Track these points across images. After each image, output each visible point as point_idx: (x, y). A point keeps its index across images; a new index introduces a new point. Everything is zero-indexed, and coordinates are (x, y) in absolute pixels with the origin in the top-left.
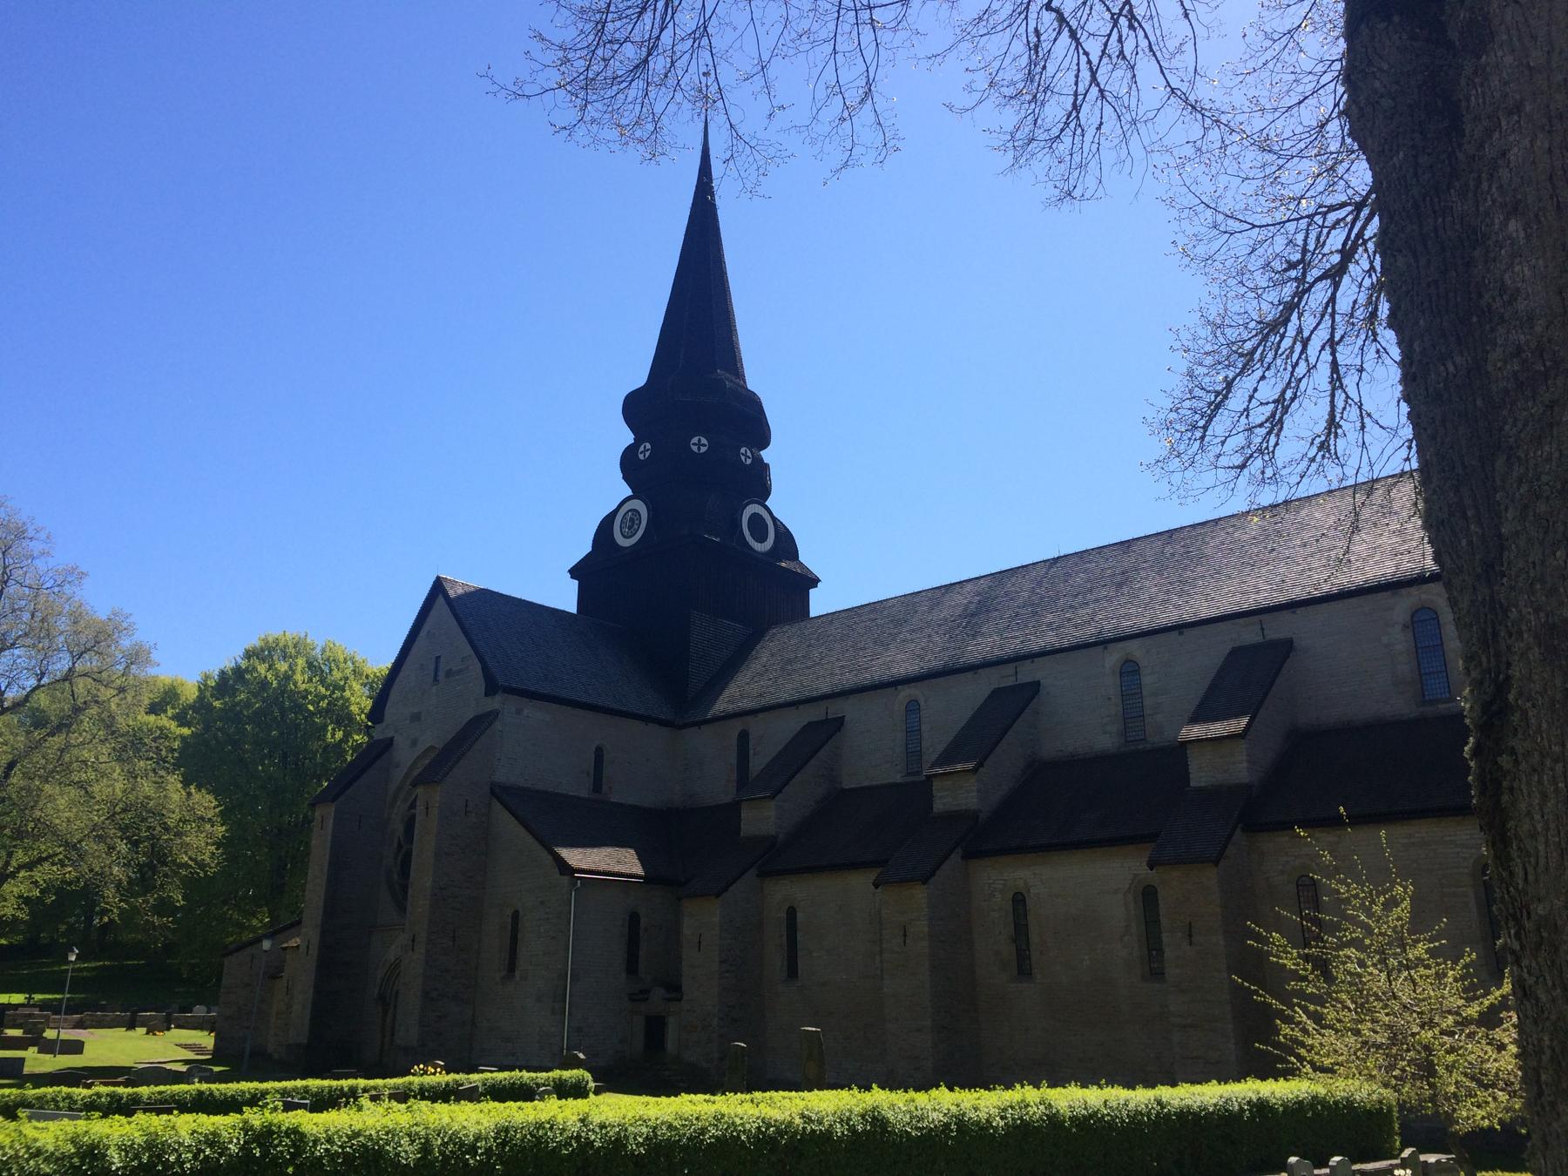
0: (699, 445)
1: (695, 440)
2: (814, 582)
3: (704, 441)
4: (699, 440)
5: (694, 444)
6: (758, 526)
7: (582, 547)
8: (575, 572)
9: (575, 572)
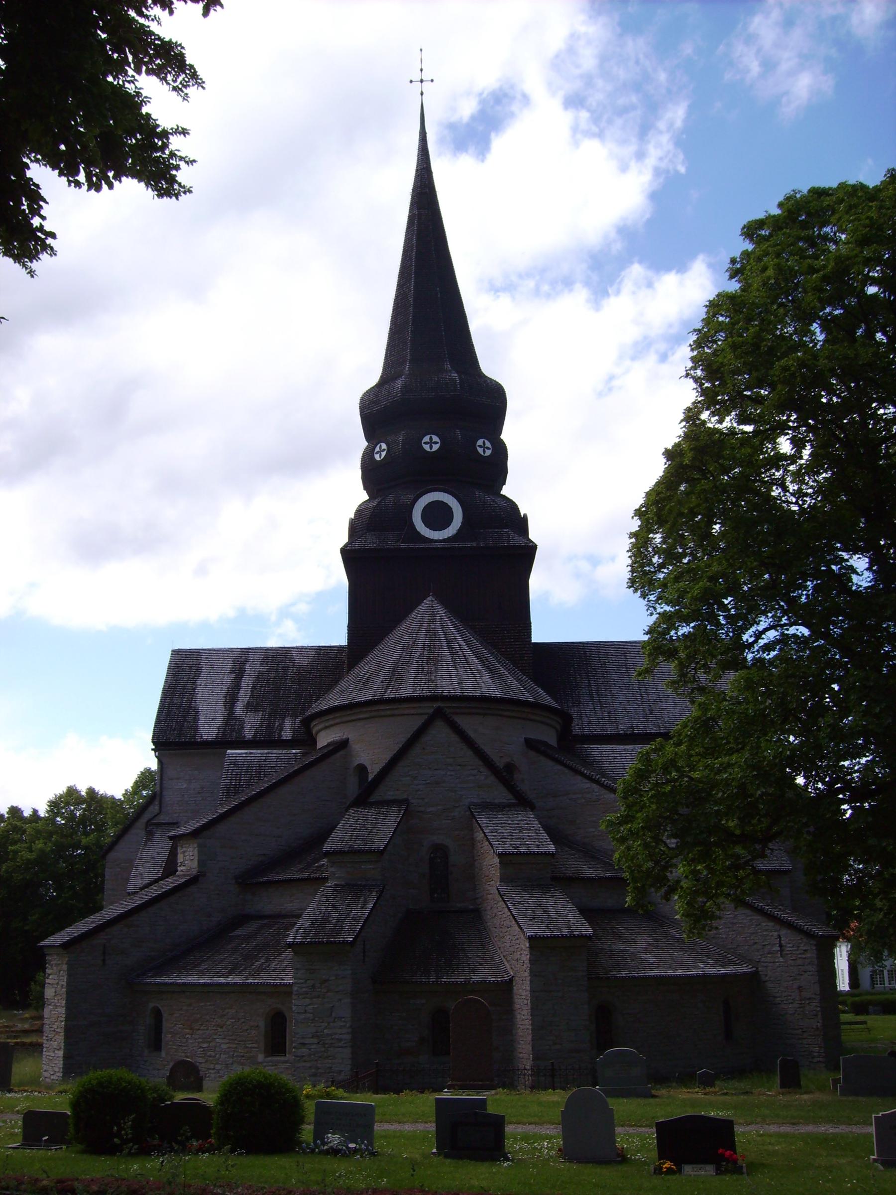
0: (431, 443)
1: (436, 447)
3: (435, 438)
4: (431, 439)
5: (436, 443)
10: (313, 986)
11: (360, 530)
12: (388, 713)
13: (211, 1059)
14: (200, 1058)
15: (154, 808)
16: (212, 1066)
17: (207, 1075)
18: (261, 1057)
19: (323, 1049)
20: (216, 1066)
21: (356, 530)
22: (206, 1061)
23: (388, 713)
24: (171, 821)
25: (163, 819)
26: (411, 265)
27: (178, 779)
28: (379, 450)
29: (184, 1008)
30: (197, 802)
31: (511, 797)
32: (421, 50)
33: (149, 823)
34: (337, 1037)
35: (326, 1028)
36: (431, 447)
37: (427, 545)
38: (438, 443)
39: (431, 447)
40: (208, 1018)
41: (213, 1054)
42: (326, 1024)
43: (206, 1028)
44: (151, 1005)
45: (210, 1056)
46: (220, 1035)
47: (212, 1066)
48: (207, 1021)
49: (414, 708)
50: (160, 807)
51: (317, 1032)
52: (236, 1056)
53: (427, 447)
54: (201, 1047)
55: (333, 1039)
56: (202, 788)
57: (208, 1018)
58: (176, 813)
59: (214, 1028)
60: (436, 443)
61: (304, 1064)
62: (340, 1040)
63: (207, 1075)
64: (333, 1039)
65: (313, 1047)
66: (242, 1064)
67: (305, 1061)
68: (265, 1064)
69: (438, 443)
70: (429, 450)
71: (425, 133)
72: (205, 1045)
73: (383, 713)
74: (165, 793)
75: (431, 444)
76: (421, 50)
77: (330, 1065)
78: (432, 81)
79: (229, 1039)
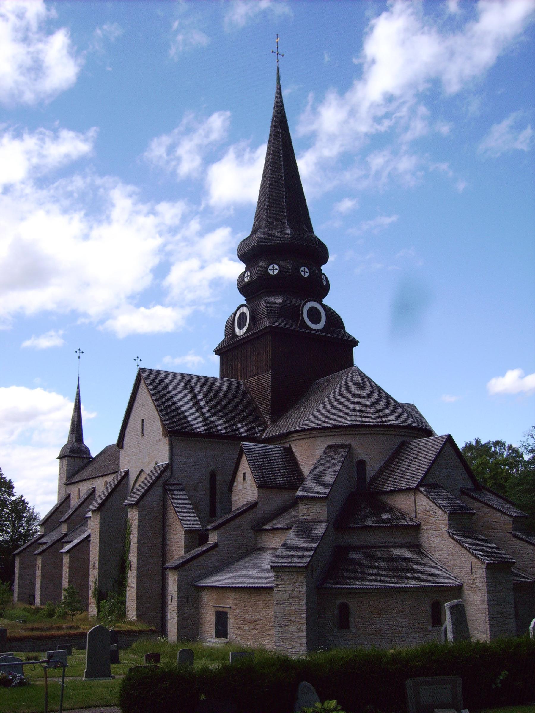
0: (273, 269)
1: (276, 272)
2: (355, 343)
3: (276, 267)
5: (276, 269)
6: (314, 315)
7: (219, 337)
8: (217, 352)
9: (217, 352)
10: (496, 586)
11: (273, 315)
12: (382, 432)
13: (396, 631)
14: (387, 631)
15: (168, 474)
16: (397, 635)
17: (393, 641)
18: (430, 628)
19: (503, 620)
20: (400, 635)
21: (270, 315)
22: (392, 633)
24: (177, 482)
25: (173, 481)
26: (280, 162)
27: (181, 456)
28: (303, 273)
29: (372, 602)
30: (192, 471)
31: (473, 485)
32: (277, 35)
33: (165, 484)
34: (509, 613)
35: (503, 608)
36: (273, 272)
37: (308, 331)
38: (277, 269)
39: (273, 272)
40: (391, 607)
41: (397, 628)
42: (503, 606)
43: (390, 613)
44: (339, 602)
45: (395, 629)
46: (401, 617)
47: (397, 635)
48: (391, 609)
49: (368, 430)
50: (172, 473)
51: (499, 611)
52: (414, 628)
53: (271, 272)
54: (387, 625)
55: (507, 614)
56: (195, 463)
57: (391, 607)
58: (180, 478)
59: (397, 613)
60: (276, 269)
61: (494, 629)
62: (510, 614)
63: (393, 641)
64: (507, 614)
65: (498, 619)
66: (419, 633)
67: (495, 627)
68: (433, 631)
69: (277, 269)
70: (272, 274)
71: (280, 86)
72: (390, 623)
73: (378, 432)
74: (174, 464)
75: (274, 270)
76: (277, 35)
77: (506, 629)
78: (283, 56)
79: (408, 619)
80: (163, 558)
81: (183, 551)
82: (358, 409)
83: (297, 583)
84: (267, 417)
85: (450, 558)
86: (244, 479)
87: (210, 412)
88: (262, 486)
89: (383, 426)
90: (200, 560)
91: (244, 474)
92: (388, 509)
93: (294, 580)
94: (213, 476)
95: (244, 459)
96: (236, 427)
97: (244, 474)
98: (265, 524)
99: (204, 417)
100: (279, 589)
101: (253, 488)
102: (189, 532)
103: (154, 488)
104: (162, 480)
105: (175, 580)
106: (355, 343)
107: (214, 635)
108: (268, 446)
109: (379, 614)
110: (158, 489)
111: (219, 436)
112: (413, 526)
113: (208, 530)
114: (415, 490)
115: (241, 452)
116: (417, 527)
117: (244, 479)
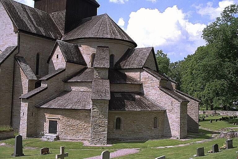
2: (98, 6)
12: (122, 43)
15: (17, 51)
23: (122, 43)
25: (19, 55)
44: (116, 117)
72: (138, 127)
80: (13, 93)
81: (27, 90)
82: (112, 32)
83: (104, 108)
84: (62, 32)
85: (159, 98)
86: (57, 57)
87: (37, 24)
88: (68, 61)
89: (123, 40)
90: (39, 95)
91: (58, 55)
92: (125, 77)
93: (102, 106)
94: (38, 55)
95: (58, 48)
96: (50, 33)
97: (58, 55)
98: (70, 79)
99: (34, 26)
100: (94, 110)
101: (63, 62)
102: (30, 81)
103: (10, 57)
104: (14, 53)
105: (26, 104)
106: (98, 6)
107: (48, 132)
108: (68, 44)
109: (134, 122)
110: (12, 58)
111: (42, 36)
112: (140, 84)
113: (41, 80)
114: (141, 70)
115: (57, 44)
116: (141, 85)
117: (57, 57)
